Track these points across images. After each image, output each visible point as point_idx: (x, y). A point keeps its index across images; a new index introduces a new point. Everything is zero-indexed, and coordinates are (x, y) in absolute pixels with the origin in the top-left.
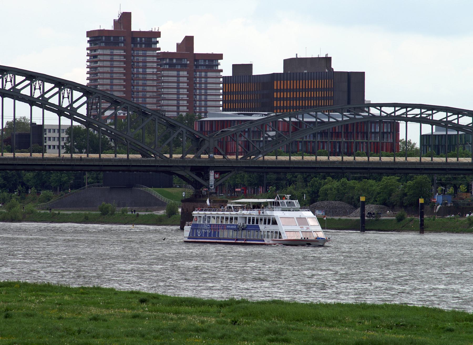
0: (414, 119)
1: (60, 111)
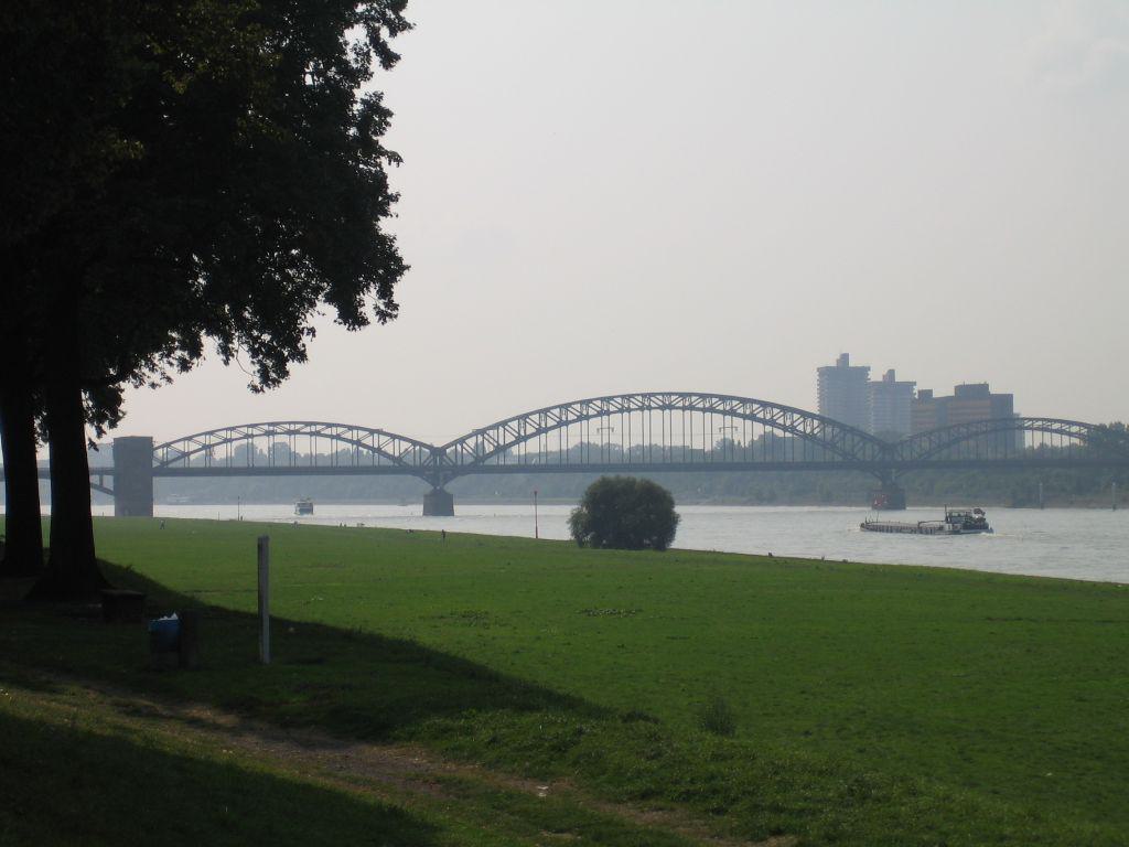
0: (1038, 429)
1: (784, 428)
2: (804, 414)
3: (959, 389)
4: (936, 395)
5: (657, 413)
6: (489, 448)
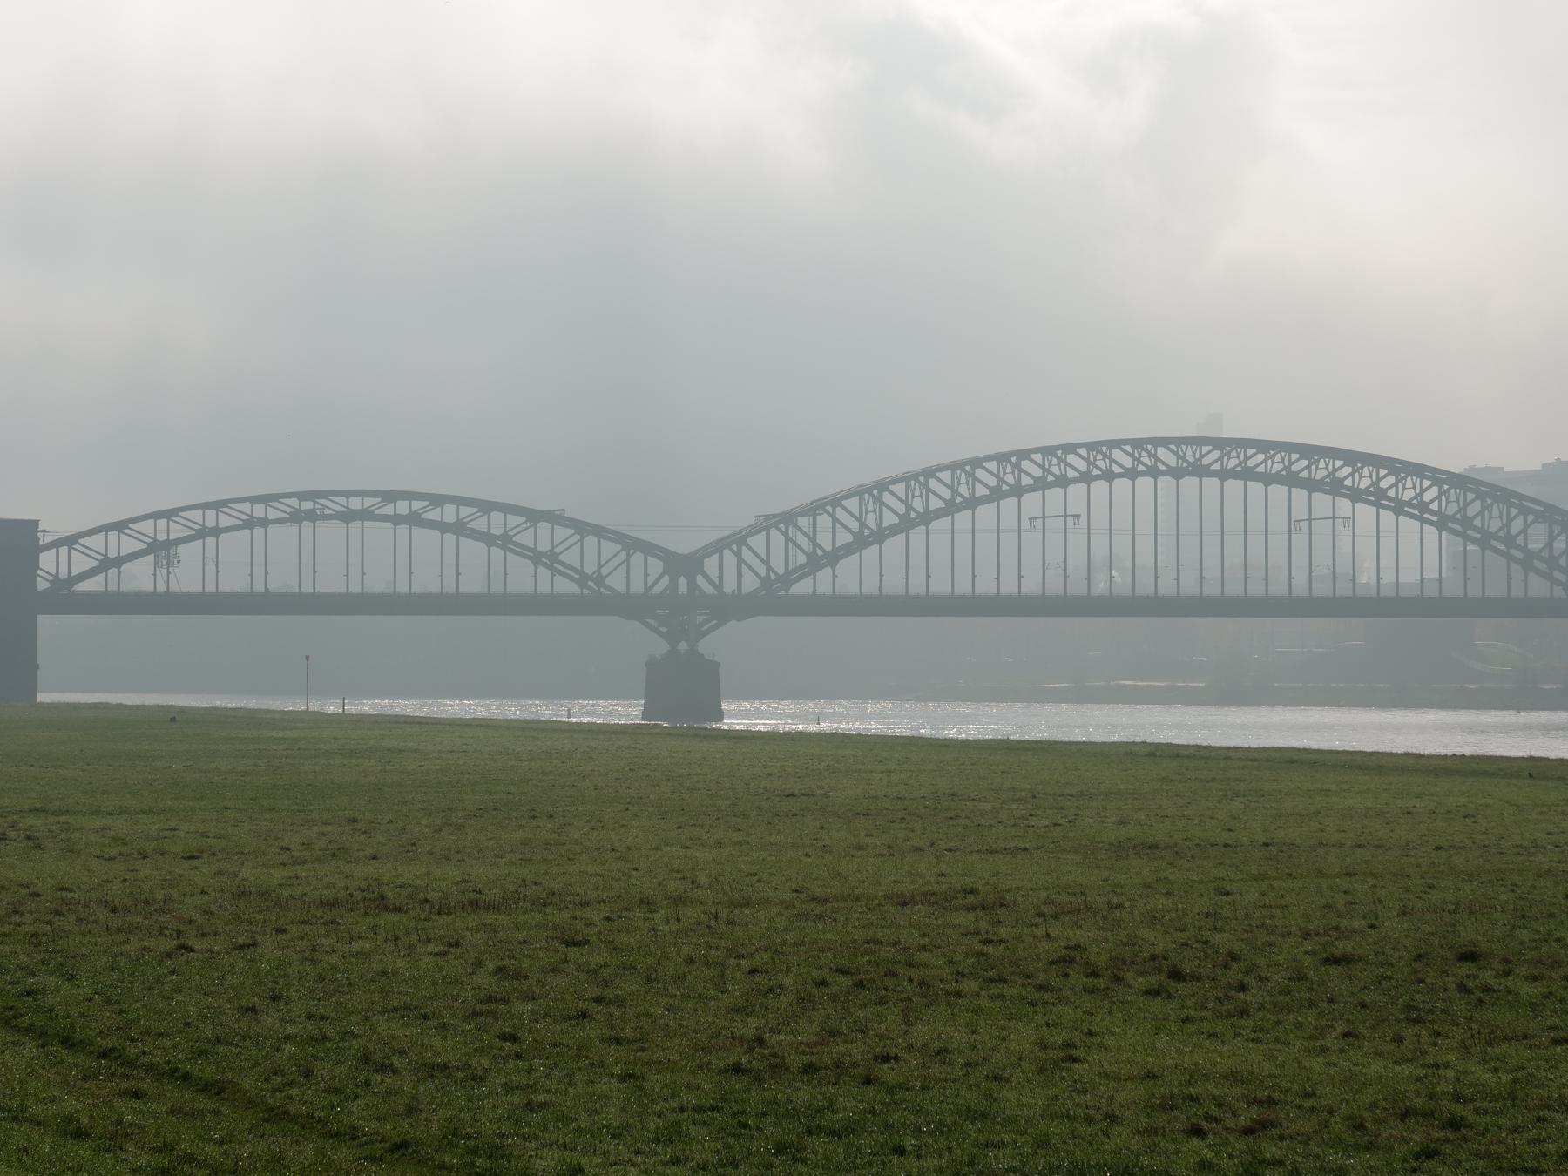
4: (1505, 470)
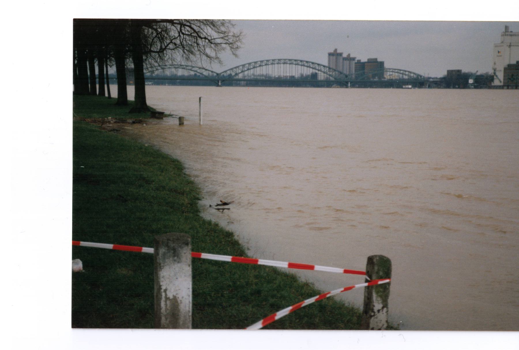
2: (324, 66)
3: (368, 60)
5: (282, 65)
6: (233, 74)
